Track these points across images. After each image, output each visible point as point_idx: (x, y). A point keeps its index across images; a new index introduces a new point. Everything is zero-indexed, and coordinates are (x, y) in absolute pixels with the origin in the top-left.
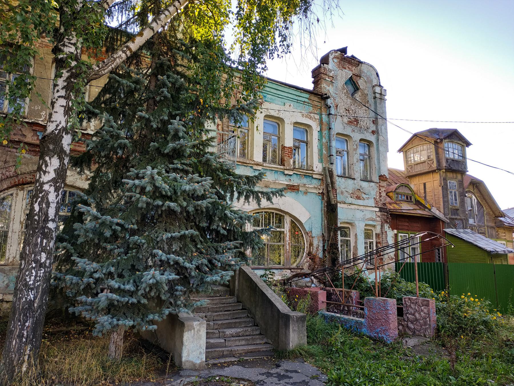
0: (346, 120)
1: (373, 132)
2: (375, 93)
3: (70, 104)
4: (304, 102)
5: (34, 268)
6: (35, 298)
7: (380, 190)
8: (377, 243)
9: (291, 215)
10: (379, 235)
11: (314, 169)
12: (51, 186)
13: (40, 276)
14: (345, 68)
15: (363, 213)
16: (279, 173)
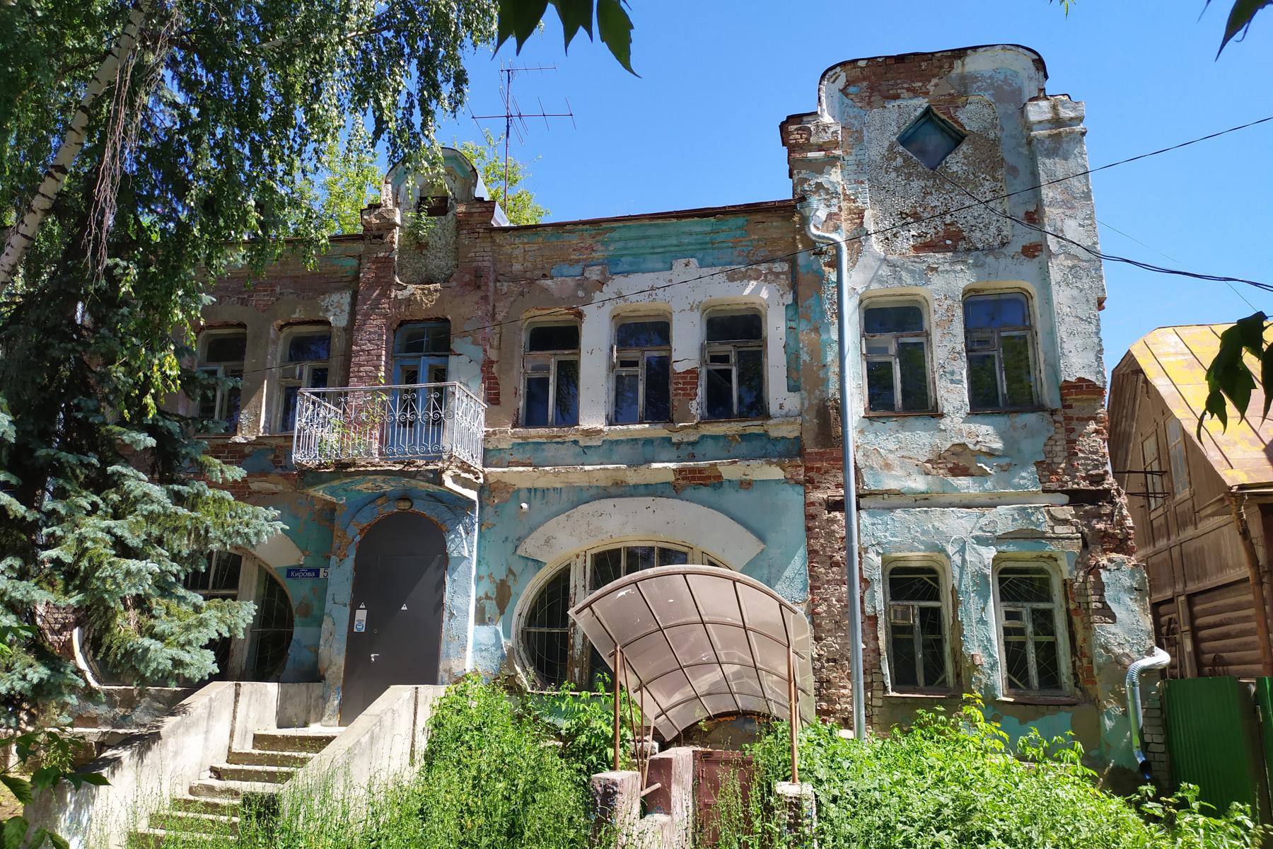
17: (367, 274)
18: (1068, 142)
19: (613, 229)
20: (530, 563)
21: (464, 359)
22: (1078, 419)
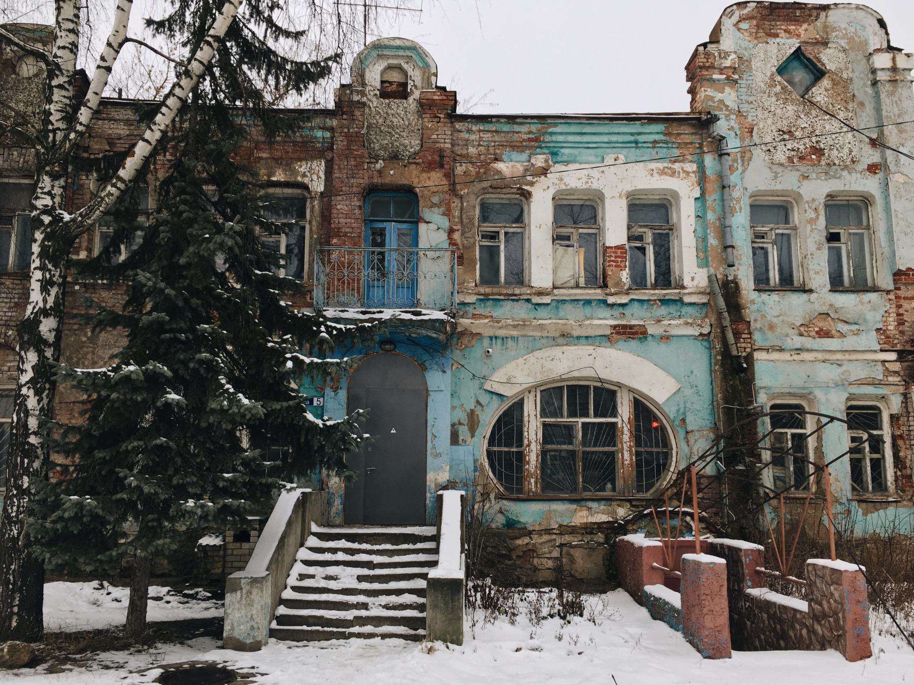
0: (781, 156)
1: (873, 169)
2: (874, 71)
3: (48, 276)
4: (655, 142)
5: (15, 496)
6: (19, 534)
7: (899, 306)
8: (894, 438)
9: (631, 390)
10: (898, 419)
11: (687, 282)
12: (29, 388)
13: (23, 507)
14: (776, 36)
15: (840, 370)
16: (594, 304)
17: (340, 144)
18: (902, 88)
19: (555, 125)
20: (494, 397)
21: (433, 226)
22: (904, 298)
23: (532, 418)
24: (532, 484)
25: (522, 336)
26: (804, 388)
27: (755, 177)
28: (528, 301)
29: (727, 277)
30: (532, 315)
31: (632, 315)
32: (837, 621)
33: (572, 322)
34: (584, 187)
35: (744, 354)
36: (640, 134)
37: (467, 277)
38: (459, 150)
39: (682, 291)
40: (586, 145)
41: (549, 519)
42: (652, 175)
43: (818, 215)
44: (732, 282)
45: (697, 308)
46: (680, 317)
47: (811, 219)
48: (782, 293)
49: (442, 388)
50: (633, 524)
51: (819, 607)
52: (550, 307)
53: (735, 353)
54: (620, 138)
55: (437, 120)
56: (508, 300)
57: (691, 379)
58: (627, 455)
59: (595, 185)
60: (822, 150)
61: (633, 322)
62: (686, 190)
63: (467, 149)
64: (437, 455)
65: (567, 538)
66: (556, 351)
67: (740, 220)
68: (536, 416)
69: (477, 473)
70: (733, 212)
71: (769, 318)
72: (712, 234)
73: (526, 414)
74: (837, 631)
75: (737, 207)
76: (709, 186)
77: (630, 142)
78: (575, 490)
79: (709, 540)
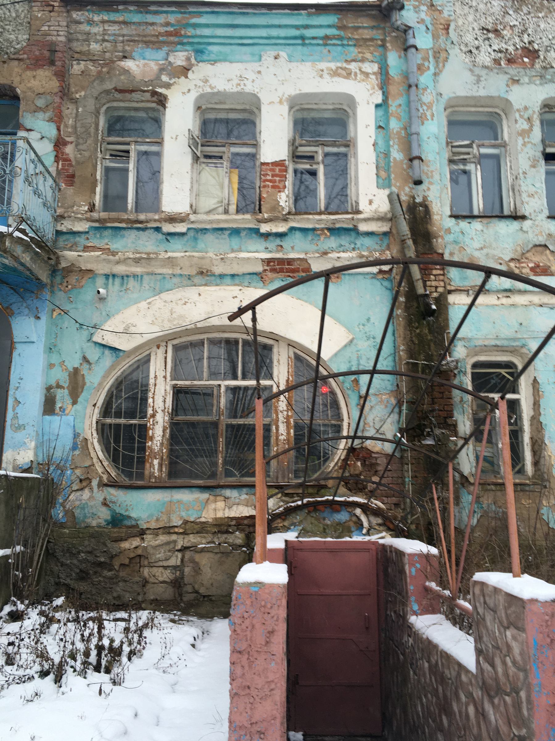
0: (485, 57)
4: (327, 37)
9: (291, 344)
11: (363, 205)
16: (243, 234)
19: (200, 14)
20: (107, 352)
23: (160, 380)
24: (155, 467)
25: (148, 274)
26: (515, 339)
27: (455, 81)
28: (158, 229)
29: (414, 198)
30: (162, 247)
31: (292, 248)
32: (517, 705)
33: (211, 254)
34: (235, 90)
35: (435, 295)
36: (307, 27)
37: (77, 199)
38: (77, 46)
39: (356, 216)
40: (240, 41)
41: (168, 513)
42: (321, 76)
43: (532, 126)
44: (421, 204)
45: (376, 239)
46: (354, 249)
47: (523, 131)
48: (485, 221)
49: (34, 338)
50: (284, 520)
51: (490, 668)
52: (186, 238)
53: (420, 290)
54: (282, 33)
55: (50, 8)
56: (131, 228)
57: (367, 329)
58: (282, 429)
59: (249, 88)
60: (537, 51)
61: (292, 256)
62: (364, 95)
63: (89, 45)
64: (19, 428)
65: (192, 539)
66: (191, 293)
67: (433, 135)
68: (165, 377)
69: (77, 452)
70: (422, 119)
71: (469, 251)
72: (396, 147)
73: (152, 375)
74: (519, 728)
75: (428, 114)
76: (393, 89)
77: (295, 38)
78: (213, 475)
79: (381, 541)
